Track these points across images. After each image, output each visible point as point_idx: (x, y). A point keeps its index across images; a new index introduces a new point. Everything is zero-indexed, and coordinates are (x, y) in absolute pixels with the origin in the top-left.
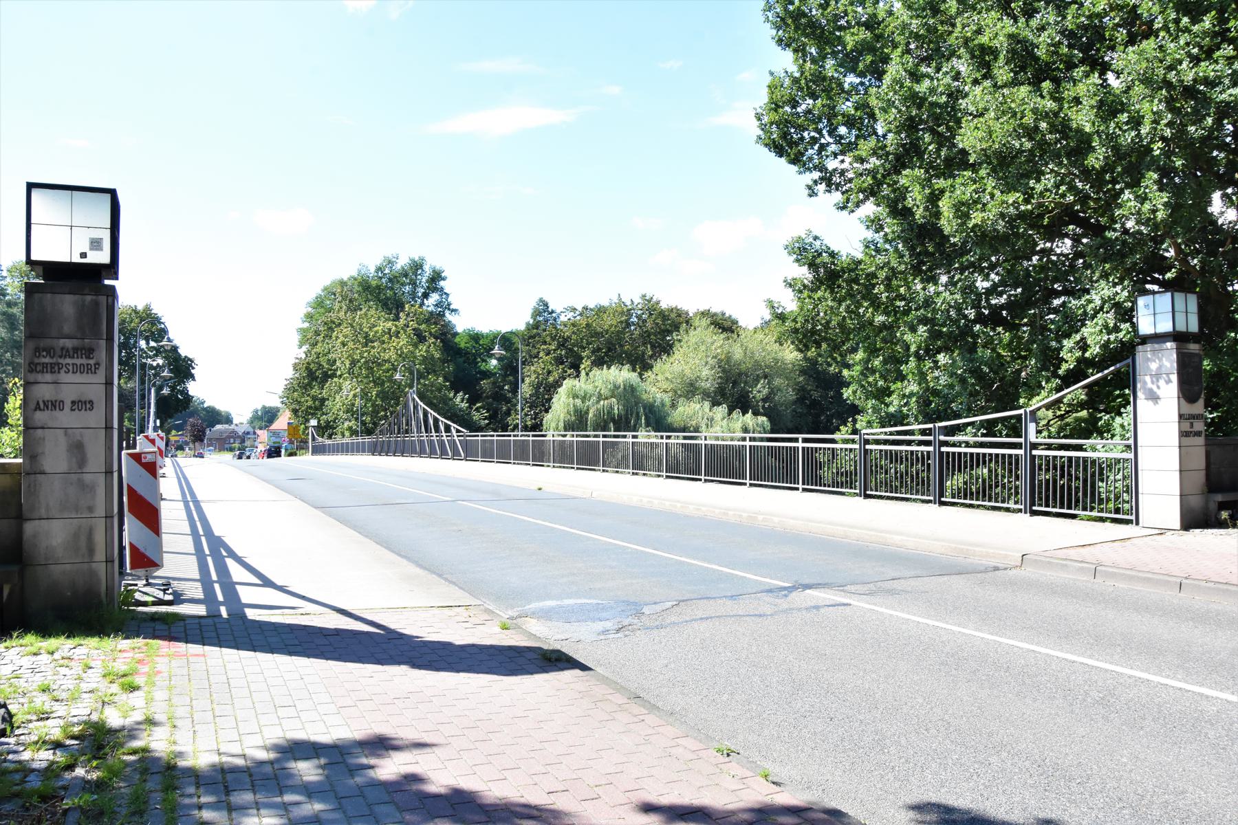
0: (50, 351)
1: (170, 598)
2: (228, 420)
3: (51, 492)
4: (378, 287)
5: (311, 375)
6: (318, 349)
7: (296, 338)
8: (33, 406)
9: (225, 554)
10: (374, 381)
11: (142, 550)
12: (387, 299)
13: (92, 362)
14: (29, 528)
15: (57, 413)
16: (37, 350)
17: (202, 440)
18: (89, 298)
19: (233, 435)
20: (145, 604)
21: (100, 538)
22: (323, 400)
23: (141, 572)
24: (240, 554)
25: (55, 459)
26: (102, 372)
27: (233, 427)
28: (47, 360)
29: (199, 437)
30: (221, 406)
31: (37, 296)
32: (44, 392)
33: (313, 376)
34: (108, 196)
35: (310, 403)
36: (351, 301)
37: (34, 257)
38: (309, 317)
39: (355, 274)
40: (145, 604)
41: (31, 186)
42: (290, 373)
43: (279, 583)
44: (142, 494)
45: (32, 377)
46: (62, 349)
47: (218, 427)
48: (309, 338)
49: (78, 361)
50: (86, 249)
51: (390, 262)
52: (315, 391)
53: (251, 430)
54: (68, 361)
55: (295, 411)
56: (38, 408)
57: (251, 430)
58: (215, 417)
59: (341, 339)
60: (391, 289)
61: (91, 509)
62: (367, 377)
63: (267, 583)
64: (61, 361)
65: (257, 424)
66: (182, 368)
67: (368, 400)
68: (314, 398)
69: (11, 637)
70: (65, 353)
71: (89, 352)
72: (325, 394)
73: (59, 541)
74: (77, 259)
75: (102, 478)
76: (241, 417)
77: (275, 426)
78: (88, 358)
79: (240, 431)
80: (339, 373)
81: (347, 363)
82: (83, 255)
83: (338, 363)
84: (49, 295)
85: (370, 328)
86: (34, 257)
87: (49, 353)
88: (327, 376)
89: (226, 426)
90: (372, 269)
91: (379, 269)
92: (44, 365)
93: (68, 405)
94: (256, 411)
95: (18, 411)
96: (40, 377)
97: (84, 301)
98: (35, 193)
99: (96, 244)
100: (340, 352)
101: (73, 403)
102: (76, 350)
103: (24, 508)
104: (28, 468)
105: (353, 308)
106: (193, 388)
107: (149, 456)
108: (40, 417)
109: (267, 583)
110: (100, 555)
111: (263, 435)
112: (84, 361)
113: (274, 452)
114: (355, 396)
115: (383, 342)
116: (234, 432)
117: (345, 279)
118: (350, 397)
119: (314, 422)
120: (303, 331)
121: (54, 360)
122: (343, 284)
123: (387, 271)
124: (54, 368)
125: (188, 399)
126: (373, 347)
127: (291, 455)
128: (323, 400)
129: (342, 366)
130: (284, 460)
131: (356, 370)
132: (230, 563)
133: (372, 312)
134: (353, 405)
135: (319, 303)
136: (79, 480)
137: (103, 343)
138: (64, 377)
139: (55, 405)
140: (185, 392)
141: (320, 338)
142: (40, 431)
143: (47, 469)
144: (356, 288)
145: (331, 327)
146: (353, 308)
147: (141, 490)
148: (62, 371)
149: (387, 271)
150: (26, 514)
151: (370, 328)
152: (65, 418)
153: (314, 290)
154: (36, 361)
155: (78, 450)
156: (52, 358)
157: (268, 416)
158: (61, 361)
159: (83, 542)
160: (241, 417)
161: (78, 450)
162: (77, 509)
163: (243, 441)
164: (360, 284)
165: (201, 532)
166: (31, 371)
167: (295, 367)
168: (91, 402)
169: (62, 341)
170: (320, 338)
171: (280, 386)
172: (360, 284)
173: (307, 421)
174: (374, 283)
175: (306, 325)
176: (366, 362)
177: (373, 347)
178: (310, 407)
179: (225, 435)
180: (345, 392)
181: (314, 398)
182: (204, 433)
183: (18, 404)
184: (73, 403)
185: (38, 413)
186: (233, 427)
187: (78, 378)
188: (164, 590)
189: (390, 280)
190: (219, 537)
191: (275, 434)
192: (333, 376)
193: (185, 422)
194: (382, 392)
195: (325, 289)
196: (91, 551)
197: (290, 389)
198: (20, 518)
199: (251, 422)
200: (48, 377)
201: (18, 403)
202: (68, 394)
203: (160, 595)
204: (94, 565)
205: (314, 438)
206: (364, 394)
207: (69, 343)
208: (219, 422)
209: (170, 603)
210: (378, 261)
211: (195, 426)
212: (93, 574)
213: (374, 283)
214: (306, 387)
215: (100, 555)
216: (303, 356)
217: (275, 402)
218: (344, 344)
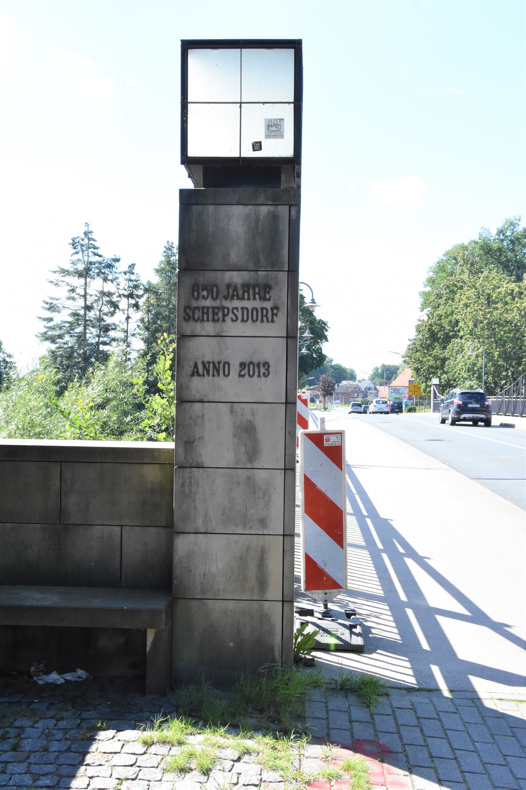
0: (212, 289)
1: (357, 641)
2: (353, 377)
3: (209, 495)
4: (500, 250)
5: (433, 336)
6: (441, 311)
7: (419, 301)
8: (188, 369)
9: (402, 550)
10: (496, 342)
11: (321, 565)
12: (508, 261)
13: (268, 305)
14: (182, 545)
15: (220, 380)
16: (195, 288)
17: (331, 394)
18: (264, 210)
19: (357, 390)
20: (325, 648)
21: (274, 564)
22: (444, 360)
23: (318, 594)
24: (421, 554)
25: (218, 447)
26: (281, 319)
27: (357, 383)
28: (208, 303)
29: (328, 392)
30: (346, 364)
31: (196, 209)
32: (204, 349)
33: (436, 338)
34: (290, 53)
35: (431, 363)
36: (472, 264)
37: (191, 153)
38: (432, 281)
39: (476, 238)
40: (325, 648)
41: (188, 46)
42: (413, 334)
43: (496, 618)
44: (323, 490)
45: (188, 328)
46: (228, 286)
47: (344, 383)
48: (430, 301)
49: (249, 304)
50: (260, 137)
51: (512, 224)
52: (437, 351)
53: (372, 386)
54: (237, 303)
55: (417, 370)
56: (195, 373)
57: (372, 386)
58: (341, 374)
59: (465, 301)
60: (513, 250)
61: (263, 522)
62: (489, 337)
63: (477, 617)
64: (227, 304)
65: (378, 380)
66: (319, 331)
67: (491, 360)
68: (436, 358)
69: (152, 727)
70: (232, 291)
71: (264, 290)
72: (446, 353)
73: (221, 566)
74: (248, 153)
75: (279, 476)
76: (363, 374)
77: (395, 383)
78: (263, 299)
79: (363, 386)
80: (461, 334)
81: (471, 324)
82: (257, 146)
83: (460, 324)
84: (211, 208)
85: (494, 289)
86: (191, 153)
87: (210, 292)
88: (448, 339)
89: (351, 382)
90: (494, 233)
91: (501, 232)
92: (205, 310)
93: (235, 369)
94: (377, 369)
95: (169, 373)
96: (198, 328)
97: (257, 215)
98: (193, 55)
99: (273, 128)
100: (466, 311)
101: (242, 365)
102: (246, 287)
103: (177, 515)
104: (182, 459)
105: (475, 272)
106: (326, 348)
107: (333, 438)
108: (199, 385)
109: (477, 617)
110: (274, 592)
111: (384, 392)
112: (257, 304)
113: (397, 408)
114: (477, 356)
115: (506, 303)
116: (357, 387)
117: (466, 244)
118: (473, 358)
119: (435, 381)
120: (426, 295)
121: (217, 303)
122: (464, 248)
123: (508, 233)
124: (217, 315)
125: (322, 358)
126: (497, 309)
127: (410, 410)
128: (444, 360)
129: (465, 327)
130: (405, 416)
131: (478, 331)
132: (410, 562)
133: (494, 274)
134: (474, 364)
135: (441, 268)
136: (249, 478)
137: (283, 276)
138: (232, 328)
139: (218, 368)
140: (319, 352)
141: (442, 301)
142: (197, 406)
143: (207, 462)
144: (477, 251)
145: (453, 290)
146: (475, 272)
147: (321, 485)
148: (228, 319)
149: (508, 233)
150: (179, 525)
151: (494, 289)
152: (231, 387)
153: (435, 253)
154: (194, 304)
155: (247, 432)
156: (215, 299)
157: (387, 374)
158: (227, 304)
159: (252, 572)
160: (363, 374)
161: (247, 432)
162: (245, 521)
163: (365, 396)
164: (482, 248)
165: (365, 513)
166: (188, 318)
167: (419, 330)
168: (266, 364)
169: (228, 274)
170: (442, 301)
171: (403, 347)
172: (482, 248)
173: (428, 379)
174: (495, 246)
175: (428, 289)
176: (488, 324)
177: (497, 309)
178: (432, 367)
179: (350, 390)
180: (467, 353)
181: (436, 358)
182: (333, 389)
183: (167, 366)
184: (242, 365)
185: (196, 380)
186: (357, 383)
187: (248, 328)
188: (351, 628)
189: (512, 242)
190: (386, 521)
191: (396, 390)
192: (455, 336)
193: (317, 378)
194: (505, 352)
195: (447, 254)
196: (263, 583)
197: (413, 349)
198: (171, 529)
199: (372, 379)
200: (209, 328)
201: (169, 363)
202: (235, 353)
203: (346, 635)
204: (266, 604)
205: (435, 396)
206: (488, 355)
207: (237, 278)
208: (345, 379)
209: (358, 650)
210: (500, 224)
211: (332, 382)
212: (264, 618)
213: (495, 246)
214: (429, 347)
215: (274, 592)
216: (426, 318)
217: (396, 361)
218: (466, 306)
